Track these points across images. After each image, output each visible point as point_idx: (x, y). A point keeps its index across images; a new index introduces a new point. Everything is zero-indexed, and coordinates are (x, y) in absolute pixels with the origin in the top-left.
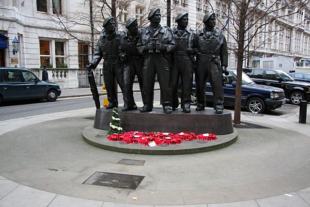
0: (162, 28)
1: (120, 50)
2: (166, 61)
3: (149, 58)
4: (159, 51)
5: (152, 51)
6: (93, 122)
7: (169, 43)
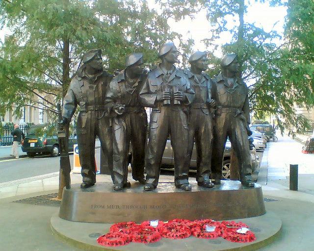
1: (108, 98)
7: (187, 91)
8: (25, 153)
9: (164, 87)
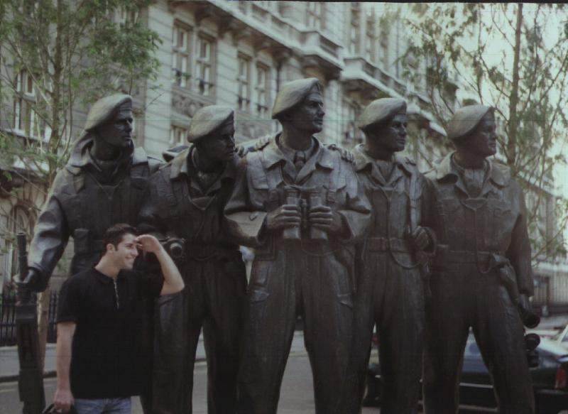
0: (323, 151)
2: (341, 270)
4: (324, 235)
5: (296, 233)
7: (349, 204)
9: (286, 193)
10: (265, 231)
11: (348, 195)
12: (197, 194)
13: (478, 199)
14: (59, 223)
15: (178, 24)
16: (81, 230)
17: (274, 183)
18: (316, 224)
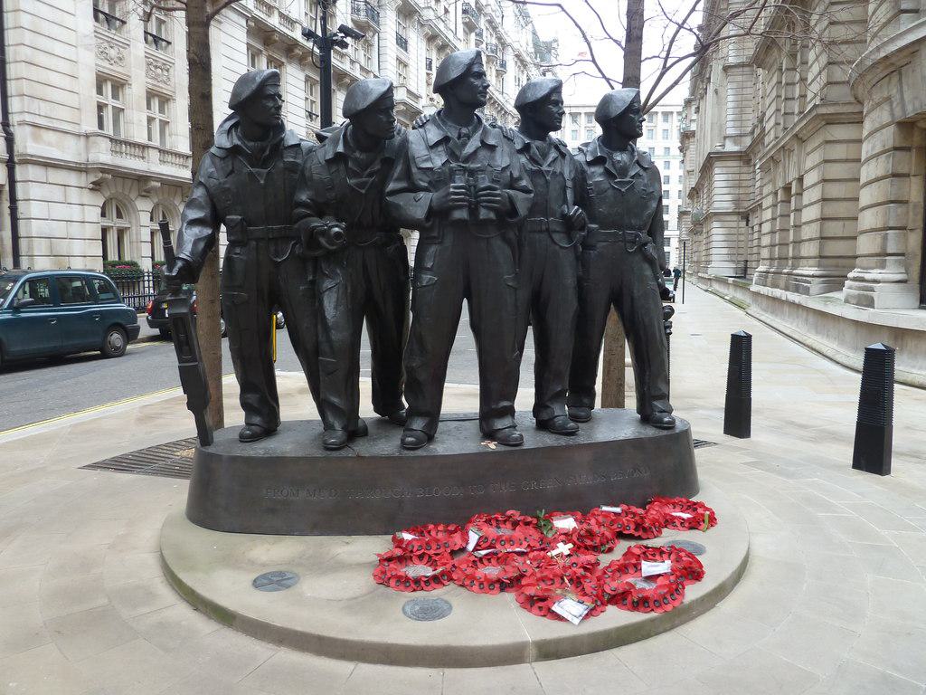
0: (485, 129)
3: (448, 241)
4: (492, 215)
6: (177, 493)
7: (512, 183)
8: (156, 331)
9: (452, 172)
10: (431, 212)
11: (511, 174)
12: (356, 175)
13: (628, 179)
14: (208, 211)
15: (308, 79)
16: (235, 217)
17: (438, 160)
18: (484, 204)
